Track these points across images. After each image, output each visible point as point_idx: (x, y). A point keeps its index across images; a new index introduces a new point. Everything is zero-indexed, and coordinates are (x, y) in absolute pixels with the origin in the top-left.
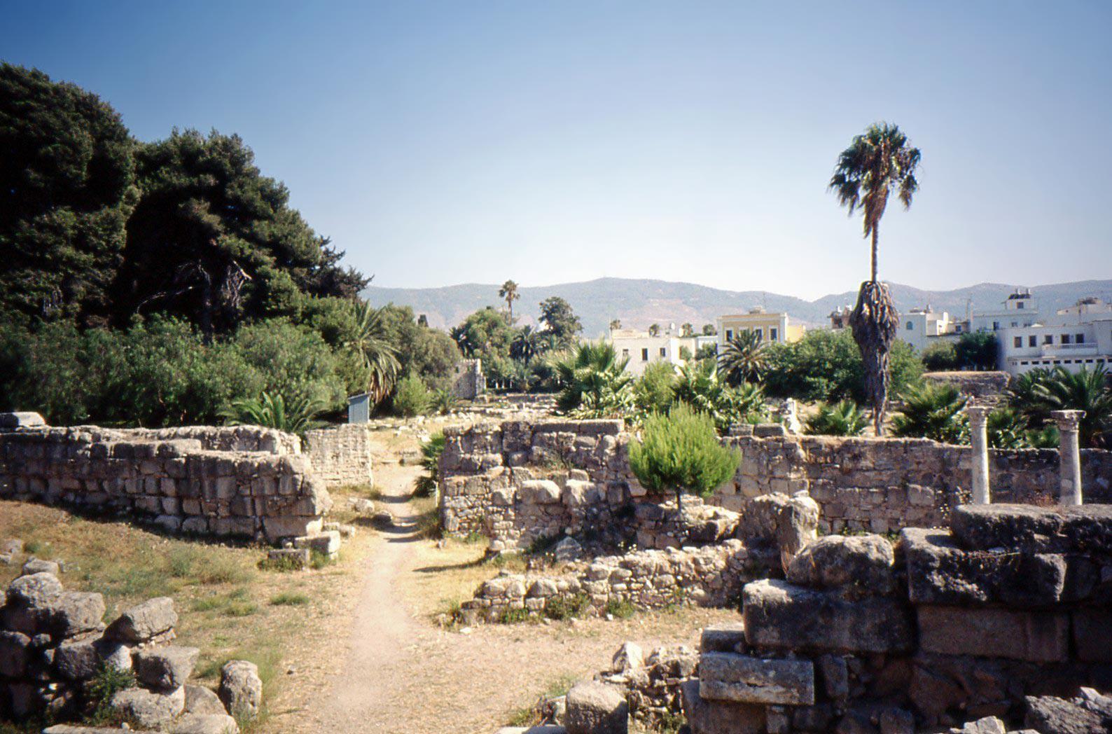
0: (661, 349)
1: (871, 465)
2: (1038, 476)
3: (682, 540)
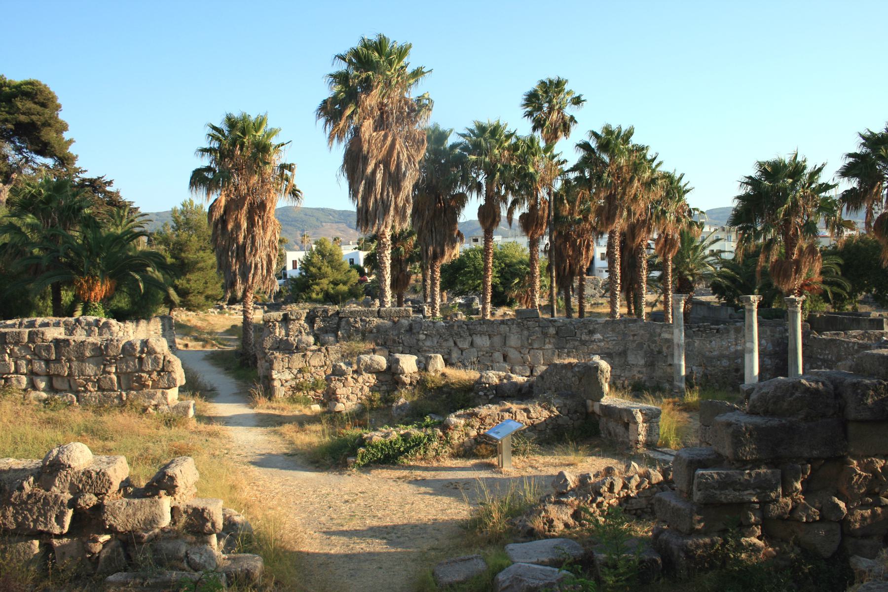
0: (293, 261)
1: (602, 338)
2: (711, 342)
3: (491, 397)
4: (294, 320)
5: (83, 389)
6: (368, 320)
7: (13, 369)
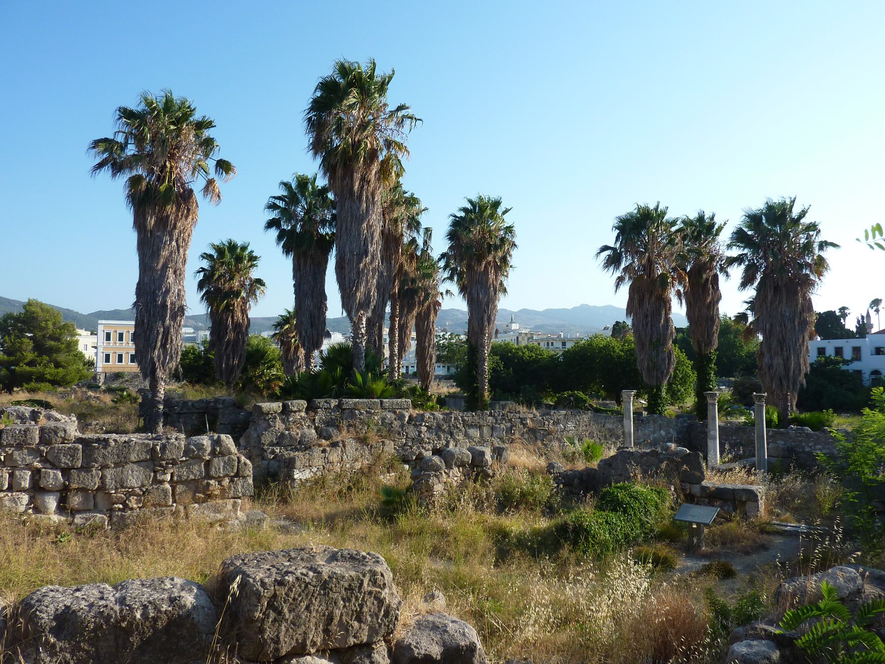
4: (295, 412)
5: (121, 506)
6: (373, 411)
7: (6, 487)
